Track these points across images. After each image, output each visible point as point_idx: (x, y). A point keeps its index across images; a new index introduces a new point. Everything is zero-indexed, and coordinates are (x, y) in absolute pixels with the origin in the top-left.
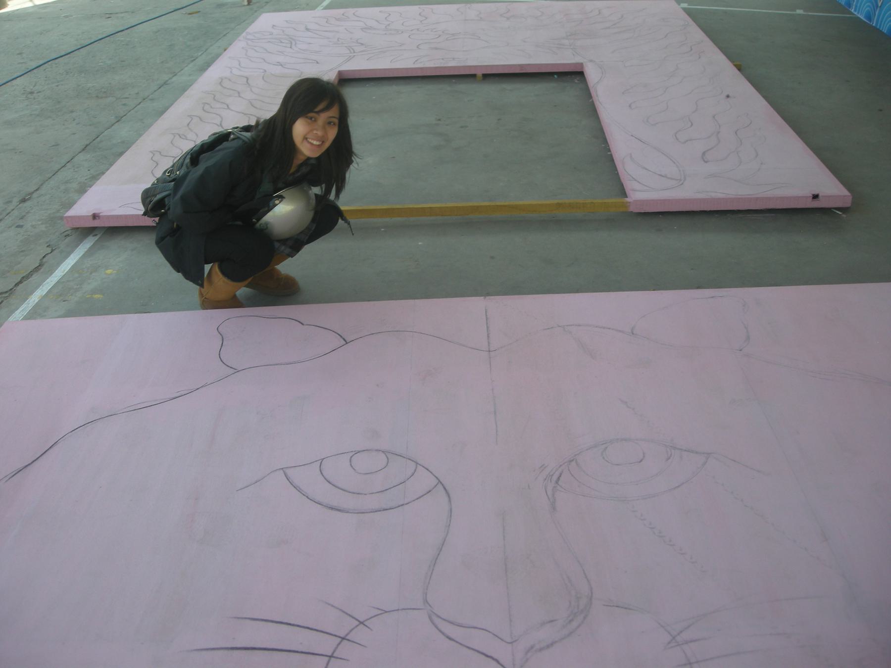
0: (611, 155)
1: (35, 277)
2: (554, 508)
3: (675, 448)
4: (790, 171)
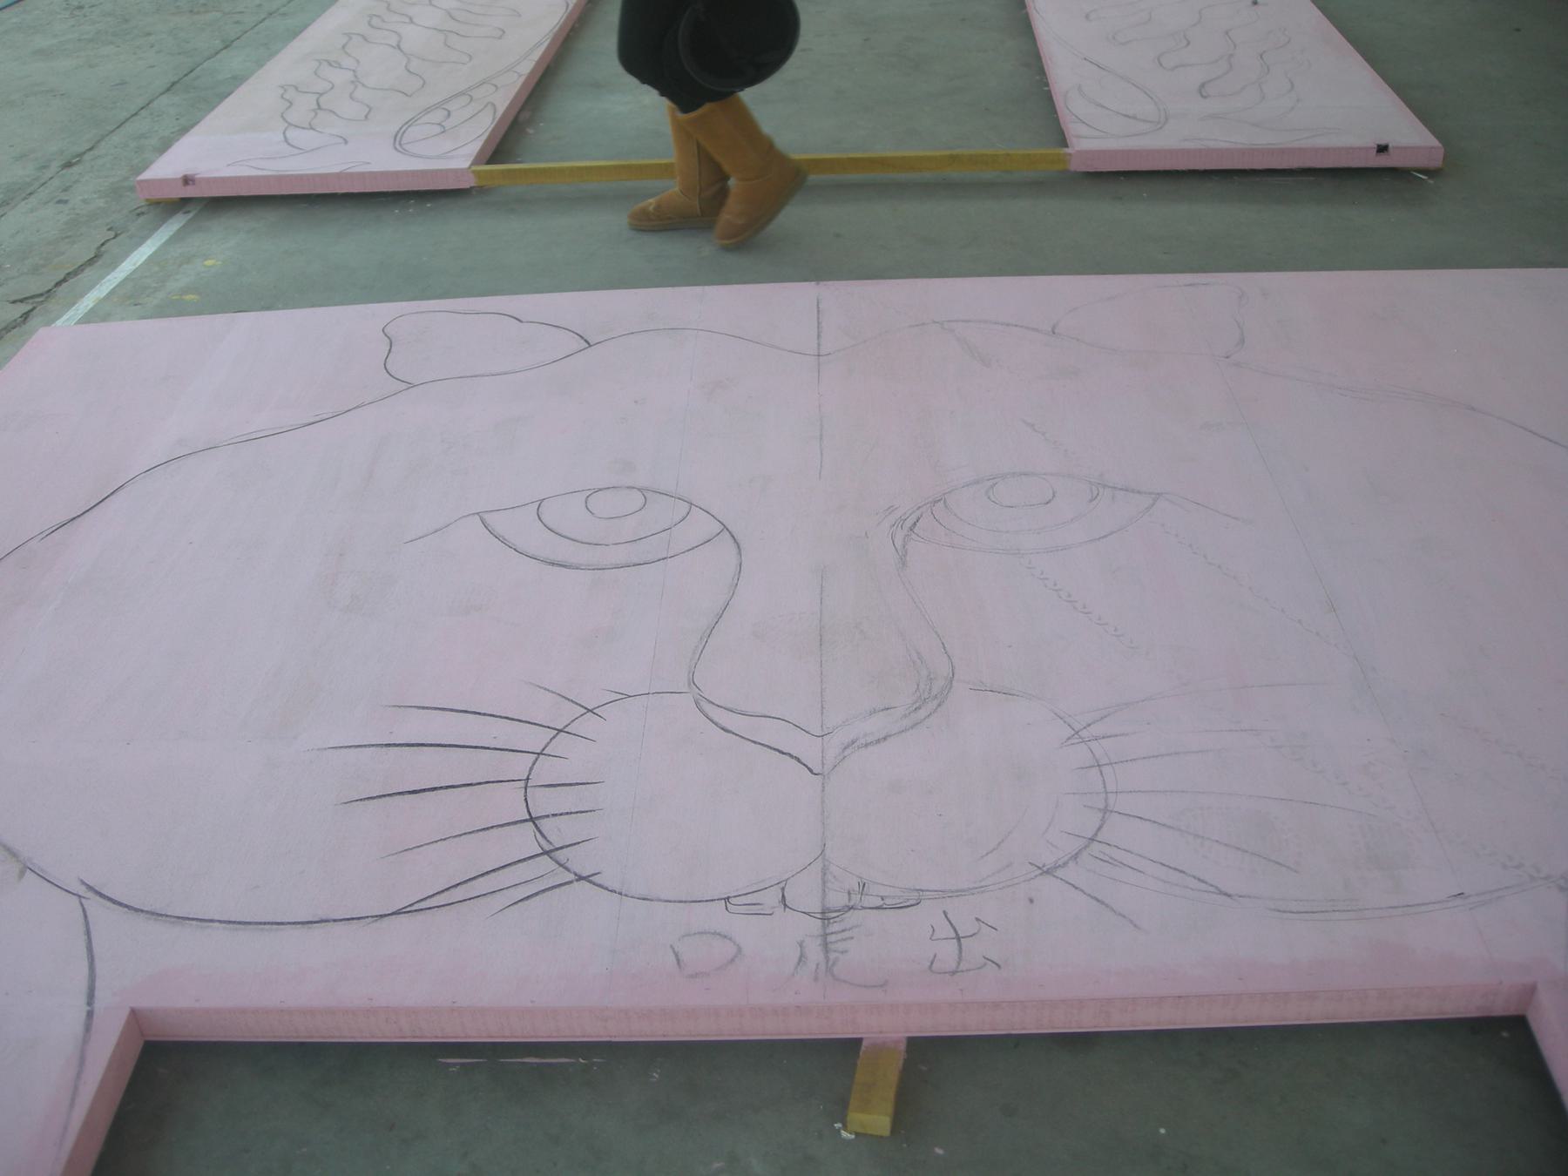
0: (1049, 92)
1: (88, 273)
2: (903, 562)
3: (1104, 486)
4: (1348, 108)
